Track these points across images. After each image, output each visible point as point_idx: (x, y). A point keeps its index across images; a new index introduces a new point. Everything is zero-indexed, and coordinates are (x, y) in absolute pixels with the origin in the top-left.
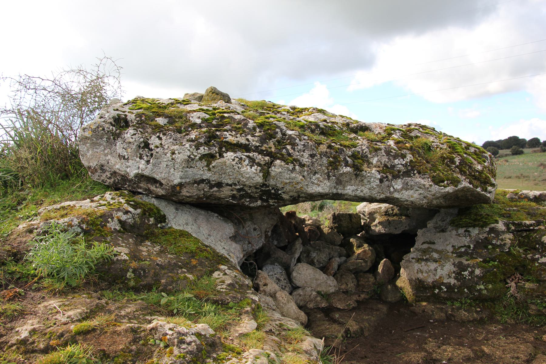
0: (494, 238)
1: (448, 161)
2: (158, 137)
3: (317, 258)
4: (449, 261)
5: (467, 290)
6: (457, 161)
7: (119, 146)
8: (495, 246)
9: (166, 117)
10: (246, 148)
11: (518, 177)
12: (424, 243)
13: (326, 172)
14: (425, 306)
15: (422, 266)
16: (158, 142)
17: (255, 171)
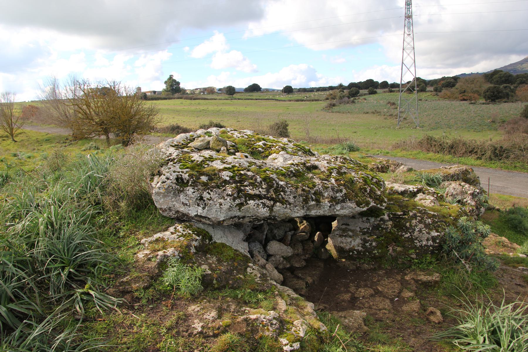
0: (382, 224)
2: (208, 192)
3: (277, 233)
6: (368, 190)
7: (182, 197)
8: (383, 228)
9: (207, 175)
10: (259, 197)
11: (373, 113)
12: (342, 224)
14: (344, 262)
16: (208, 196)
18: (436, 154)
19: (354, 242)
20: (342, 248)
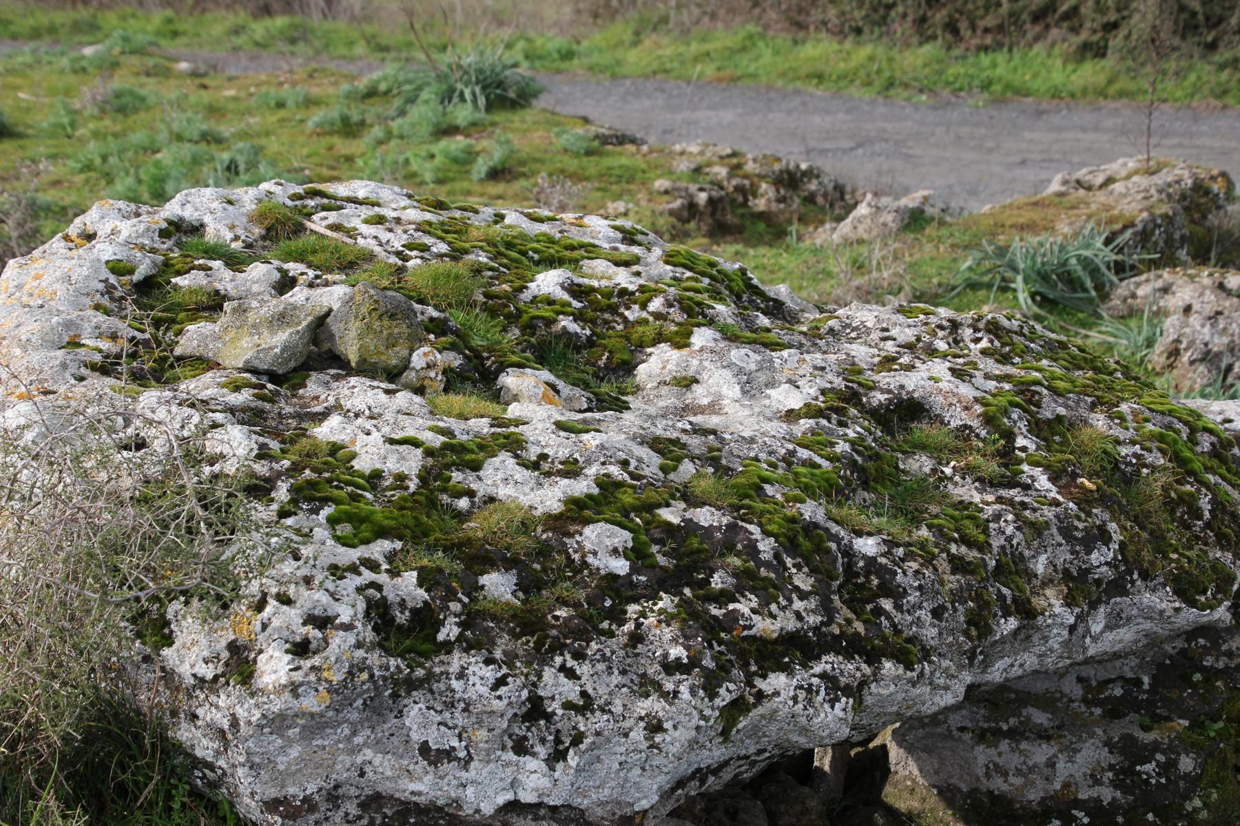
0: (1206, 651)
1: (1184, 513)
2: (563, 668)
4: (1092, 735)
5: (1155, 816)
6: (1205, 503)
8: (1211, 674)
9: (510, 563)
13: (967, 648)
15: (1000, 754)
16: (570, 689)
17: (841, 714)
18: (848, 45)
19: (1071, 760)
20: (997, 799)
